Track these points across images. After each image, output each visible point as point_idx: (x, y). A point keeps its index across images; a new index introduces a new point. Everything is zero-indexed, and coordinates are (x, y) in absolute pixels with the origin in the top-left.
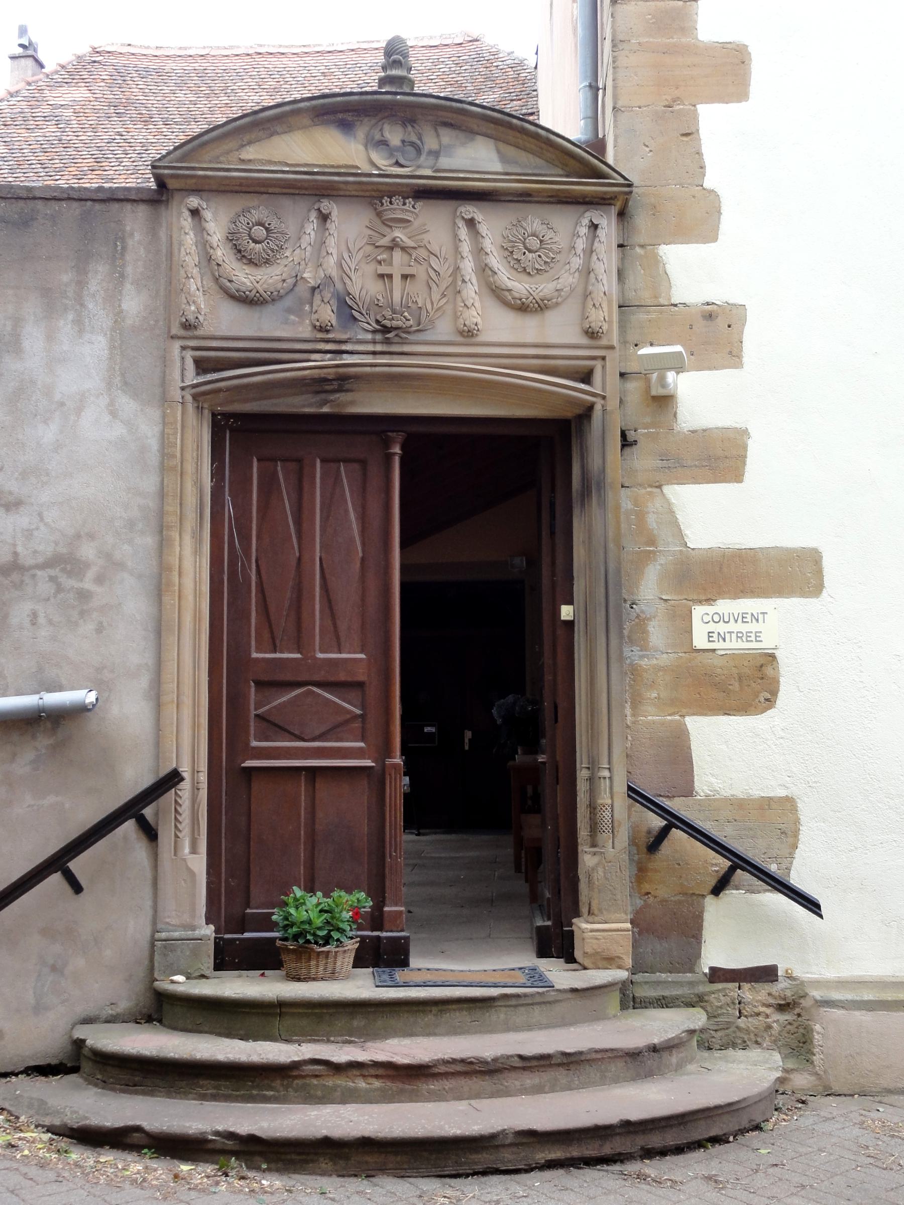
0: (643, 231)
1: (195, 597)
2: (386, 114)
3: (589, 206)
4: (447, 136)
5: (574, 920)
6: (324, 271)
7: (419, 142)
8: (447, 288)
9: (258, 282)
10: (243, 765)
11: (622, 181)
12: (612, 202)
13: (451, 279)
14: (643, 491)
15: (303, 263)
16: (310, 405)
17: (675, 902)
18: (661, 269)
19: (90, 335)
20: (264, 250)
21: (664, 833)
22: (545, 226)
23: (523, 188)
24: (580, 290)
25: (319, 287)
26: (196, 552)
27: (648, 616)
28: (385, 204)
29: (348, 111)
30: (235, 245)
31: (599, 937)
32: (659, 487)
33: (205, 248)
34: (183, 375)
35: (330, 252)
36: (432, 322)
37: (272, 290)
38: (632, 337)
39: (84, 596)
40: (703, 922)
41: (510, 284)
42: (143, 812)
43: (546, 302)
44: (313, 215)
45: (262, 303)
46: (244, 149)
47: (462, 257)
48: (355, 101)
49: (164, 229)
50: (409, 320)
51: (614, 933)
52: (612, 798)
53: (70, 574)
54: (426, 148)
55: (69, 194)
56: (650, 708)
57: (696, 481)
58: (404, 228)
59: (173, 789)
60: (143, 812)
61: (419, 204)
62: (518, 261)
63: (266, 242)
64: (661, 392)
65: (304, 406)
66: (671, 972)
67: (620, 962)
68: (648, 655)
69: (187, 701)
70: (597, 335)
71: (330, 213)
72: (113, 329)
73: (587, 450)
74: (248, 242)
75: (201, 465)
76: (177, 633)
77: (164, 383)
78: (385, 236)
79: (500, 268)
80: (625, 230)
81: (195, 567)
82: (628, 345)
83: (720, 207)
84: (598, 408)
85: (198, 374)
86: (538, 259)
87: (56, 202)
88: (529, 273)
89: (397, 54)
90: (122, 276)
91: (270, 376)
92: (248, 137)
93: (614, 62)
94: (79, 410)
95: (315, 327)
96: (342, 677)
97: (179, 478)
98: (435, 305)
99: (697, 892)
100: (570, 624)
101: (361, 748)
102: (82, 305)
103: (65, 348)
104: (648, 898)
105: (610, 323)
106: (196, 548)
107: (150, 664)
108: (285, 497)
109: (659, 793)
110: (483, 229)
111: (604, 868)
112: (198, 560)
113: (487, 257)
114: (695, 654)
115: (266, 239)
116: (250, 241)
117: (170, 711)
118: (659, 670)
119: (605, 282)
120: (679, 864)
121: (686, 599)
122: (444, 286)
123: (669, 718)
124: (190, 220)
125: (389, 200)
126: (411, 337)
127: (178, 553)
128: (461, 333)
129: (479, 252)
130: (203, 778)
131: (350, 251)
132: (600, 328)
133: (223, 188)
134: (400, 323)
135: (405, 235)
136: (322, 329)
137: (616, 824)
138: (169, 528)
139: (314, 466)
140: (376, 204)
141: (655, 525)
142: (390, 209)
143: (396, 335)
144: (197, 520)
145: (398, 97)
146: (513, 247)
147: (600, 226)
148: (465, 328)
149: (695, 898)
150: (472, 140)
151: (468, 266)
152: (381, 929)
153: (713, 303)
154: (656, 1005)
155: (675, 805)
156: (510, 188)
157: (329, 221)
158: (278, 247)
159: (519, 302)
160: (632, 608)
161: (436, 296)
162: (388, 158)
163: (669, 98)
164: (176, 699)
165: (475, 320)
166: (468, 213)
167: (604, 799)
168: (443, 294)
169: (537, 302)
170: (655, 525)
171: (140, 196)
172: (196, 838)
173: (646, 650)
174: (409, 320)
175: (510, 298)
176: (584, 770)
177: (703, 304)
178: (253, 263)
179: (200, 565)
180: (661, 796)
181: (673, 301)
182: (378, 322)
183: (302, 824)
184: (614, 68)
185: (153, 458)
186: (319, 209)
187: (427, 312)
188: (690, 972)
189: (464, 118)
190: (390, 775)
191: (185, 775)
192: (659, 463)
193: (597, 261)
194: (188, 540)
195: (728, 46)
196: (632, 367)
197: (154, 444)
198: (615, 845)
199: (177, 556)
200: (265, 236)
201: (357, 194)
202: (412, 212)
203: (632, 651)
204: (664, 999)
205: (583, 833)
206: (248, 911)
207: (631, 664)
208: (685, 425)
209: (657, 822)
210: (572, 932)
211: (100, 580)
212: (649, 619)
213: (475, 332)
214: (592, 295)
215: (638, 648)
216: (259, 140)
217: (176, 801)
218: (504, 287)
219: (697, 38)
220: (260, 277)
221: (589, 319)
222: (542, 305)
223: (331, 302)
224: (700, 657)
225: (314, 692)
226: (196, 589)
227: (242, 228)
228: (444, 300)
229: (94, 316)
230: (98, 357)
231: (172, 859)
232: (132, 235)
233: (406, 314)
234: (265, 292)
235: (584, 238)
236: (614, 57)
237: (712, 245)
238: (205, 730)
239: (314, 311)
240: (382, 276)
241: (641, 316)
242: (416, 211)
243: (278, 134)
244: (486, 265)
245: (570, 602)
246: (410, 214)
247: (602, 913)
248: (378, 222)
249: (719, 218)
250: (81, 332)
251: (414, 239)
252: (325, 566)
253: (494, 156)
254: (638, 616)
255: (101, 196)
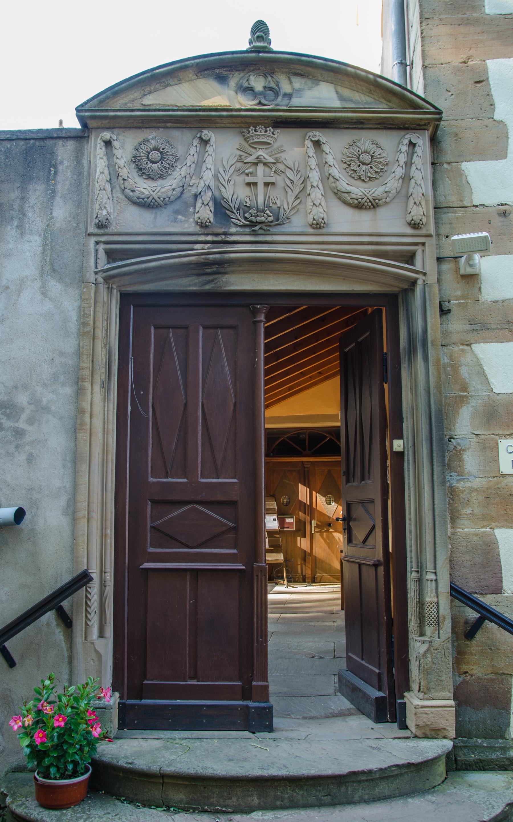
0: (449, 152)
1: (104, 434)
2: (252, 68)
3: (407, 131)
4: (298, 83)
5: (406, 694)
6: (204, 181)
7: (276, 88)
8: (299, 192)
9: (154, 191)
10: (141, 567)
11: (433, 110)
12: (425, 127)
13: (302, 186)
14: (456, 349)
15: (188, 176)
16: (195, 285)
17: (488, 679)
18: (464, 180)
19: (29, 236)
20: (158, 168)
21: (478, 625)
22: (374, 146)
23: (357, 117)
24: (403, 192)
25: (200, 194)
26: (105, 398)
27: (463, 448)
28: (251, 132)
29: (223, 67)
30: (137, 165)
31: (429, 712)
32: (469, 345)
33: (112, 166)
34: (96, 263)
35: (209, 168)
36: (287, 218)
37: (165, 197)
38: (444, 230)
39: (19, 433)
40: (511, 696)
41: (349, 188)
42: (62, 604)
43: (377, 201)
44: (196, 142)
45: (157, 207)
46: (146, 97)
47: (311, 169)
48: (228, 58)
49: (86, 157)
50: (270, 216)
51: (441, 709)
52: (437, 597)
53: (9, 417)
54: (282, 92)
55: (17, 136)
56: (466, 522)
57: (498, 340)
58: (266, 149)
59: (84, 587)
60: (62, 604)
61: (277, 131)
62: (355, 171)
63: (160, 162)
64: (469, 271)
65: (190, 285)
66: (485, 738)
67: (445, 733)
68: (464, 479)
69: (96, 516)
70: (418, 226)
71: (209, 140)
72: (45, 231)
73: (412, 316)
74: (147, 163)
75: (110, 332)
76: (88, 462)
77: (82, 269)
78: (251, 155)
79: (341, 176)
80: (435, 152)
81: (104, 411)
82: (440, 236)
83: (507, 133)
84: (420, 282)
85: (108, 263)
86: (370, 170)
87: (9, 142)
88: (363, 180)
89: (260, 32)
90: (54, 192)
91: (163, 262)
92: (148, 89)
93: (422, 33)
94: (19, 293)
95: (197, 223)
96: (220, 497)
97: (92, 341)
98: (290, 206)
99: (507, 672)
100: (400, 455)
101: (234, 554)
102: (24, 215)
103: (11, 246)
104: (466, 676)
105: (428, 217)
106: (105, 396)
107: (67, 487)
108: (176, 356)
109: (474, 591)
110: (326, 148)
111: (432, 654)
112: (106, 405)
113: (330, 168)
114: (501, 478)
115: (161, 160)
116: (149, 162)
117: (83, 524)
118: (474, 491)
119: (423, 186)
120: (491, 649)
121: (493, 434)
122: (297, 191)
123: (482, 530)
124: (104, 149)
125: (254, 128)
126: (273, 230)
127: (90, 399)
128: (311, 225)
129: (322, 165)
130: (110, 577)
131: (224, 167)
132: (421, 220)
133: (129, 125)
134: (263, 219)
135: (267, 154)
136: (203, 225)
137: (441, 619)
138: (83, 380)
139: (198, 332)
140: (244, 132)
141: (466, 375)
142: (255, 135)
143: (261, 228)
144: (106, 374)
145: (261, 54)
146: (351, 161)
147: (417, 145)
148: (314, 222)
149: (504, 677)
150: (317, 85)
151: (315, 176)
152: (250, 698)
153: (506, 204)
154: (474, 767)
155: (488, 600)
156: (348, 118)
157: (208, 146)
158: (169, 165)
159: (356, 201)
160: (450, 441)
161: (291, 199)
162: (253, 100)
163: (464, 57)
164: (87, 515)
165: (322, 216)
166: (315, 137)
167: (429, 598)
168: (296, 197)
169: (370, 201)
170: (466, 375)
171: (69, 134)
172: (104, 625)
173: (462, 476)
174: (270, 216)
175: (349, 198)
176: (413, 573)
177: (498, 205)
178: (151, 178)
179: (104, 408)
180: (476, 593)
181: (475, 203)
182: (246, 218)
183: (188, 613)
184: (422, 38)
185: (73, 326)
186: (201, 138)
187: (285, 210)
188: (501, 739)
189: (310, 69)
190: (257, 576)
191: (93, 575)
192: (469, 327)
193: (416, 171)
194: (97, 388)
195: (509, 16)
196: (447, 252)
197: (74, 316)
198: (441, 636)
199: (90, 402)
200: (160, 158)
201: (228, 125)
202: (272, 137)
203: (451, 476)
204: (481, 762)
205: (413, 625)
206: (145, 682)
207: (451, 487)
208: (488, 297)
209: (473, 615)
210: (405, 703)
211: (31, 421)
212: (464, 450)
213: (322, 225)
214: (413, 196)
215: (456, 474)
216: (157, 90)
217: (86, 596)
218: (343, 190)
219: (484, 12)
220: (155, 188)
221: (412, 214)
222: (374, 204)
223: (209, 204)
224: (506, 481)
225: (197, 509)
226: (104, 428)
227: (143, 153)
228: (298, 201)
229: (32, 222)
230: (34, 251)
231: (84, 643)
232: (62, 162)
233: (268, 212)
234: (159, 198)
235: (406, 154)
236: (422, 30)
237: (504, 161)
238: (111, 538)
239: (196, 211)
240: (249, 184)
241: (450, 215)
242: (275, 136)
243: (171, 85)
244: (330, 174)
245: (401, 437)
246: (271, 139)
247: (430, 691)
248: (246, 145)
249: (507, 142)
250: (22, 234)
251: (273, 157)
252: (206, 409)
253: (334, 95)
254: (455, 447)
255: (40, 135)
